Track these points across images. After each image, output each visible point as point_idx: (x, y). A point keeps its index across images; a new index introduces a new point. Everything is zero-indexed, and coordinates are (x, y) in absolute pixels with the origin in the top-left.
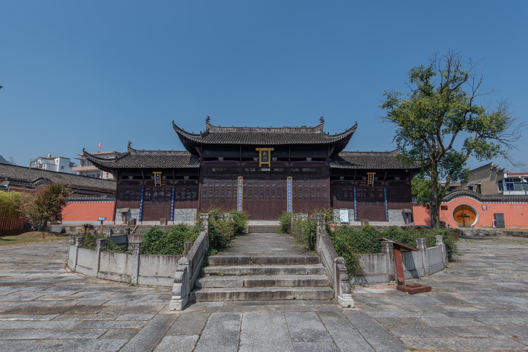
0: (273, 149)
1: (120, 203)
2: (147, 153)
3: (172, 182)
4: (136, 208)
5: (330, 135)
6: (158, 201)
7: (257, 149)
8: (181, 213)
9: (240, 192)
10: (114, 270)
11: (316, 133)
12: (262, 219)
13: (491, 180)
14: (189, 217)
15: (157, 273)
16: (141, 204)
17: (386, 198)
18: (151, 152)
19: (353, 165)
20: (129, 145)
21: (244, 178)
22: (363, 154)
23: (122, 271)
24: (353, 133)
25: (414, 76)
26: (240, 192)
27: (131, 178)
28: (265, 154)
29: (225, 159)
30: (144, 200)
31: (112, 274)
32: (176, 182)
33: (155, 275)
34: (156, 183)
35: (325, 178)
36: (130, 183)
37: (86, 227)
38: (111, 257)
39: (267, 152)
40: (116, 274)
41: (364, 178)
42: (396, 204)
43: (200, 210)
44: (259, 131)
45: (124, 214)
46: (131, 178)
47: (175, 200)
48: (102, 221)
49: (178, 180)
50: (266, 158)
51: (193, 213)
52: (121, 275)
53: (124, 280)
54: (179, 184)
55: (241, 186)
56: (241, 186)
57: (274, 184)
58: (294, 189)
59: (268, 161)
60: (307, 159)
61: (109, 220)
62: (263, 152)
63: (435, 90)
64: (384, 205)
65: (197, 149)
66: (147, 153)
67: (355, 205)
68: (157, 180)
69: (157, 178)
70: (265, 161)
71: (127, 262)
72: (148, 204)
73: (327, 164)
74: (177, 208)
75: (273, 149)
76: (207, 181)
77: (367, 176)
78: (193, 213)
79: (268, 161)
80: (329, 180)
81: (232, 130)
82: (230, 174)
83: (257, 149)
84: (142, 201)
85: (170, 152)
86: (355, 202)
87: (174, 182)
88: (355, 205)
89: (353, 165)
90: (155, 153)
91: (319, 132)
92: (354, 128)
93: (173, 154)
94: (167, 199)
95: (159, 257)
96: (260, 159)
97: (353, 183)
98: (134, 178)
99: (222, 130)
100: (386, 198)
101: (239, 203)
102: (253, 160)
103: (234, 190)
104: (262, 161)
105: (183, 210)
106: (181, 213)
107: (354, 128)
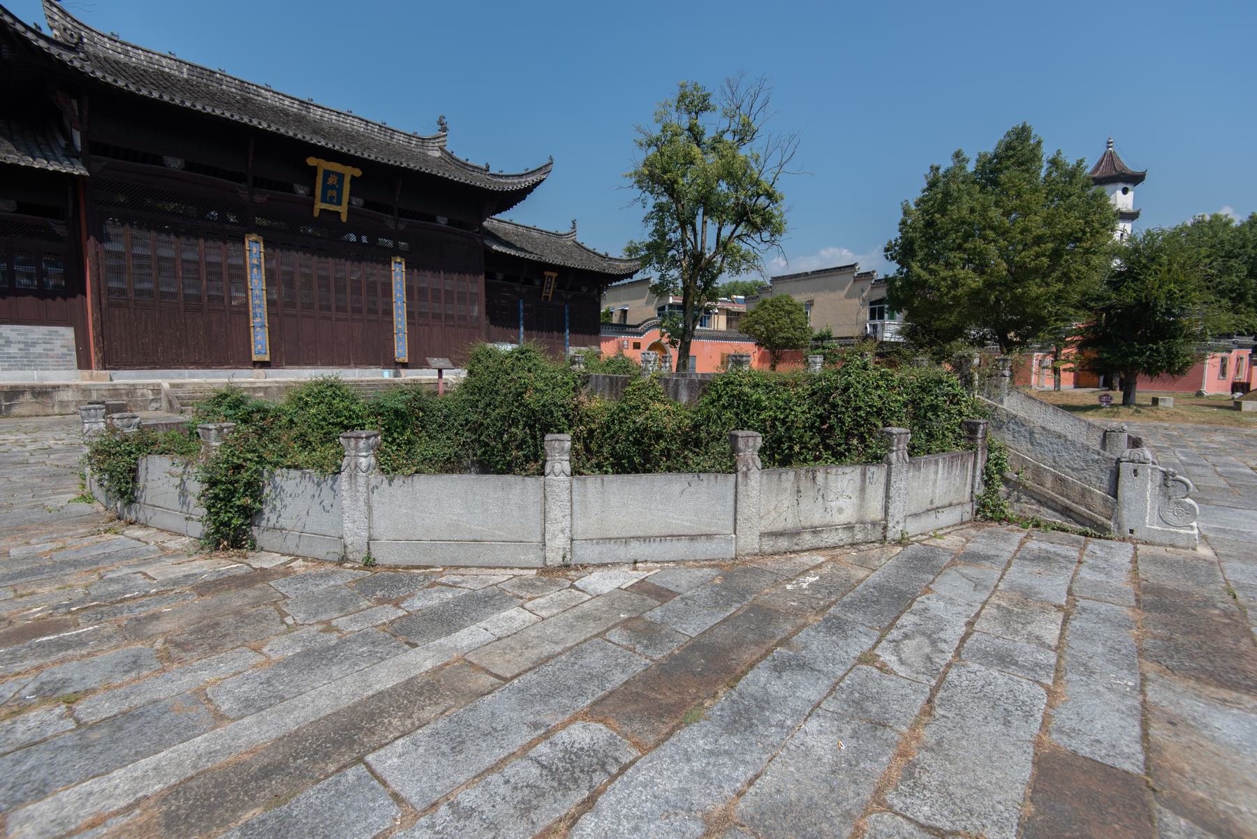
0: (358, 173)
5: (491, 171)
7: (311, 161)
9: (257, 283)
10: (817, 519)
11: (430, 153)
12: (306, 364)
13: (647, 303)
15: (932, 502)
19: (522, 250)
21: (267, 244)
22: (520, 229)
23: (849, 515)
24: (541, 181)
26: (257, 283)
28: (332, 180)
31: (815, 531)
33: (929, 507)
35: (477, 274)
38: (805, 484)
39: (341, 177)
40: (830, 527)
41: (537, 282)
42: (580, 337)
43: (693, 336)
44: (272, 100)
48: (440, 371)
50: (334, 193)
52: (849, 527)
53: (859, 536)
56: (259, 267)
59: (339, 203)
60: (439, 218)
62: (327, 174)
63: (705, 139)
70: (331, 202)
71: (863, 489)
73: (478, 241)
75: (358, 173)
76: (121, 231)
77: (543, 278)
79: (339, 203)
80: (482, 277)
81: (168, 66)
83: (311, 161)
86: (522, 329)
89: (522, 250)
91: (437, 154)
92: (545, 169)
95: (937, 462)
96: (318, 192)
97: (518, 289)
99: (126, 53)
101: (255, 316)
103: (239, 276)
104: (324, 200)
107: (545, 169)
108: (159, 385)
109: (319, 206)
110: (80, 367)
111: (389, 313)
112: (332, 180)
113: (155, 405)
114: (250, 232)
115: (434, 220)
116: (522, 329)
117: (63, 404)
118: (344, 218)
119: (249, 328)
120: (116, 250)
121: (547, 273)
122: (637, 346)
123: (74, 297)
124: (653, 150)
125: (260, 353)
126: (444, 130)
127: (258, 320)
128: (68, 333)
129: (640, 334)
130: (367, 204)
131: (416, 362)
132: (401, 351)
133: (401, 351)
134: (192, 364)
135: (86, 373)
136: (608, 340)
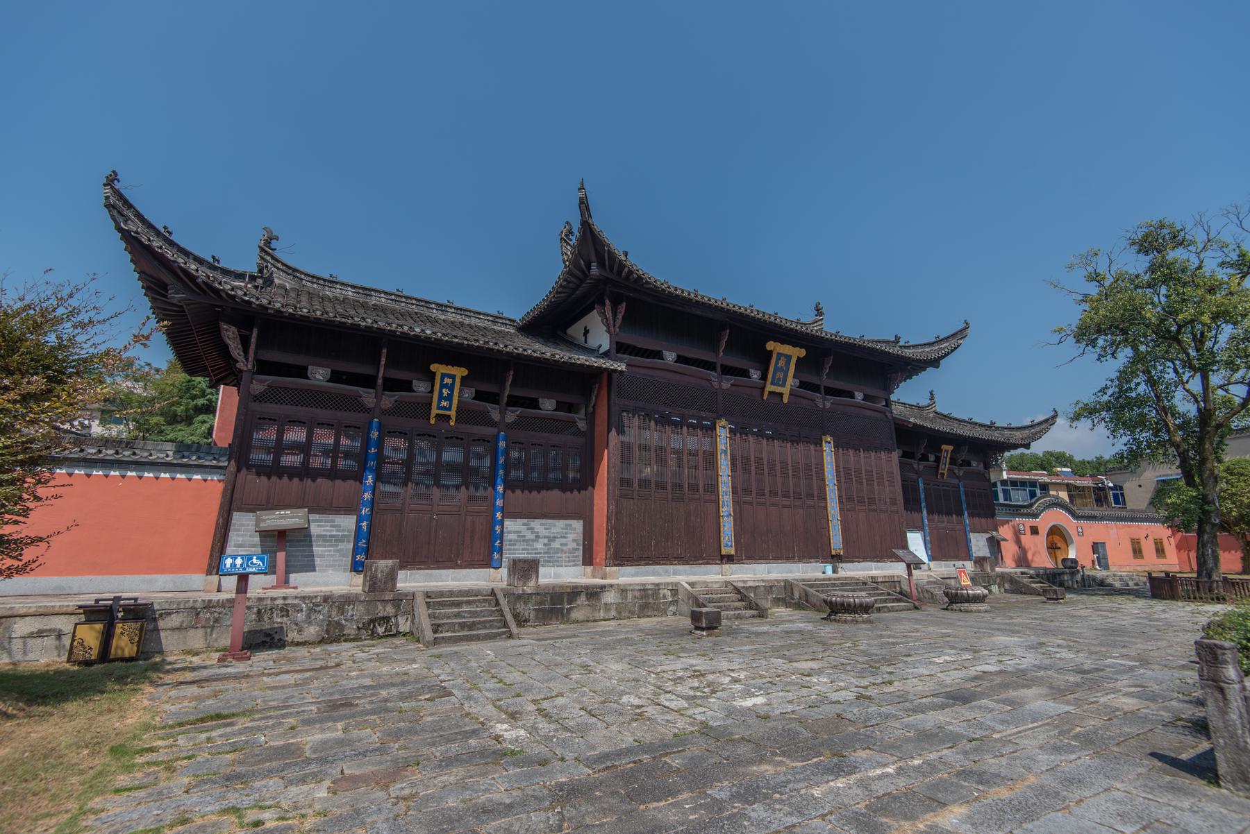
1: (255, 484)
2: (350, 293)
3: (496, 416)
4: (338, 511)
6: (437, 484)
7: (770, 346)
8: (529, 536)
12: (761, 558)
14: (558, 551)
16: (367, 496)
17: (964, 506)
18: (367, 291)
20: (268, 243)
25: (1148, 243)
27: (319, 375)
28: (782, 363)
29: (681, 359)
30: (379, 478)
32: (510, 417)
34: (435, 411)
36: (315, 397)
37: (103, 614)
39: (789, 357)
45: (277, 539)
46: (319, 375)
47: (510, 485)
49: (519, 411)
51: (571, 537)
54: (518, 424)
55: (725, 452)
57: (791, 453)
58: (843, 474)
59: (783, 385)
61: (182, 567)
62: (779, 355)
64: (963, 523)
65: (230, 335)
66: (350, 293)
67: (926, 522)
68: (441, 397)
69: (448, 388)
72: (395, 495)
74: (514, 516)
75: (802, 353)
78: (571, 537)
82: (693, 410)
83: (770, 346)
84: (369, 480)
85: (442, 307)
87: (503, 414)
88: (926, 522)
90: (383, 300)
92: (961, 333)
93: (452, 317)
94: (472, 479)
98: (336, 377)
100: (964, 506)
102: (411, 390)
103: (710, 460)
105: (537, 524)
106: (529, 536)
107: (961, 333)
108: (676, 584)
109: (770, 388)
110: (585, 563)
111: (823, 497)
112: (447, 380)
113: (673, 608)
114: (719, 418)
115: (852, 396)
116: (925, 512)
117: (607, 607)
118: (785, 400)
119: (719, 517)
120: (631, 445)
121: (944, 447)
122: (1034, 531)
123: (586, 489)
124: (1086, 306)
125: (727, 546)
126: (821, 314)
127: (725, 509)
128: (578, 525)
129: (1035, 516)
130: (479, 396)
131: (852, 554)
132: (836, 542)
133: (836, 542)
134: (676, 559)
135: (589, 569)
136: (1004, 523)
